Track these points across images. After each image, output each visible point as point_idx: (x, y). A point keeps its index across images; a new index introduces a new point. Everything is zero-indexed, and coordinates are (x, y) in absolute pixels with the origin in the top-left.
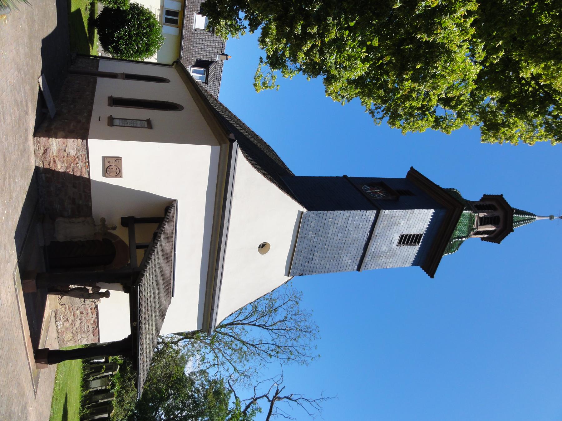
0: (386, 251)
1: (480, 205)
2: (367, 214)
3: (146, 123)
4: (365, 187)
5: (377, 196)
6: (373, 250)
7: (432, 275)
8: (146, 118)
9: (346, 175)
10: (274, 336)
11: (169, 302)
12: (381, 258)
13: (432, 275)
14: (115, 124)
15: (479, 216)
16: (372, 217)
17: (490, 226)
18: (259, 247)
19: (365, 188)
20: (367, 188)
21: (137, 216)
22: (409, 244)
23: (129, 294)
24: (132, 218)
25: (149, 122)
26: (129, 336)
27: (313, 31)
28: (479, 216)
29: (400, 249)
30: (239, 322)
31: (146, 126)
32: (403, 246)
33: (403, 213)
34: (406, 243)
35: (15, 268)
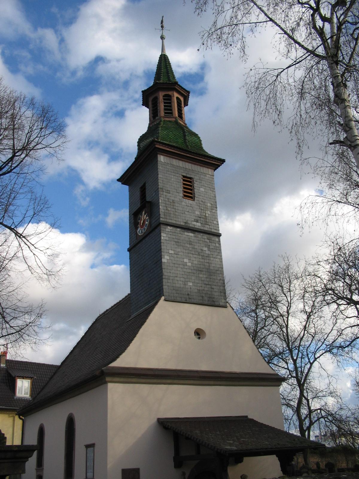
0: (200, 210)
1: (153, 107)
2: (161, 176)
3: (89, 449)
4: (139, 232)
5: (147, 223)
6: (200, 224)
7: (223, 161)
8: (84, 449)
9: (128, 249)
10: (295, 299)
11: (252, 420)
12: (207, 215)
13: (223, 161)
14: (92, 477)
15: (163, 116)
16: (170, 228)
17: (173, 104)
18: (199, 338)
19: (140, 231)
20: (140, 230)
21: (172, 454)
22: (192, 180)
23: (244, 458)
24: (175, 459)
25: (87, 446)
26: (277, 456)
27: (198, 432)
28: (163, 116)
29: (198, 196)
30: (284, 334)
31: (92, 448)
32: (194, 193)
33: (161, 165)
34: (192, 191)
35: (141, 96)
